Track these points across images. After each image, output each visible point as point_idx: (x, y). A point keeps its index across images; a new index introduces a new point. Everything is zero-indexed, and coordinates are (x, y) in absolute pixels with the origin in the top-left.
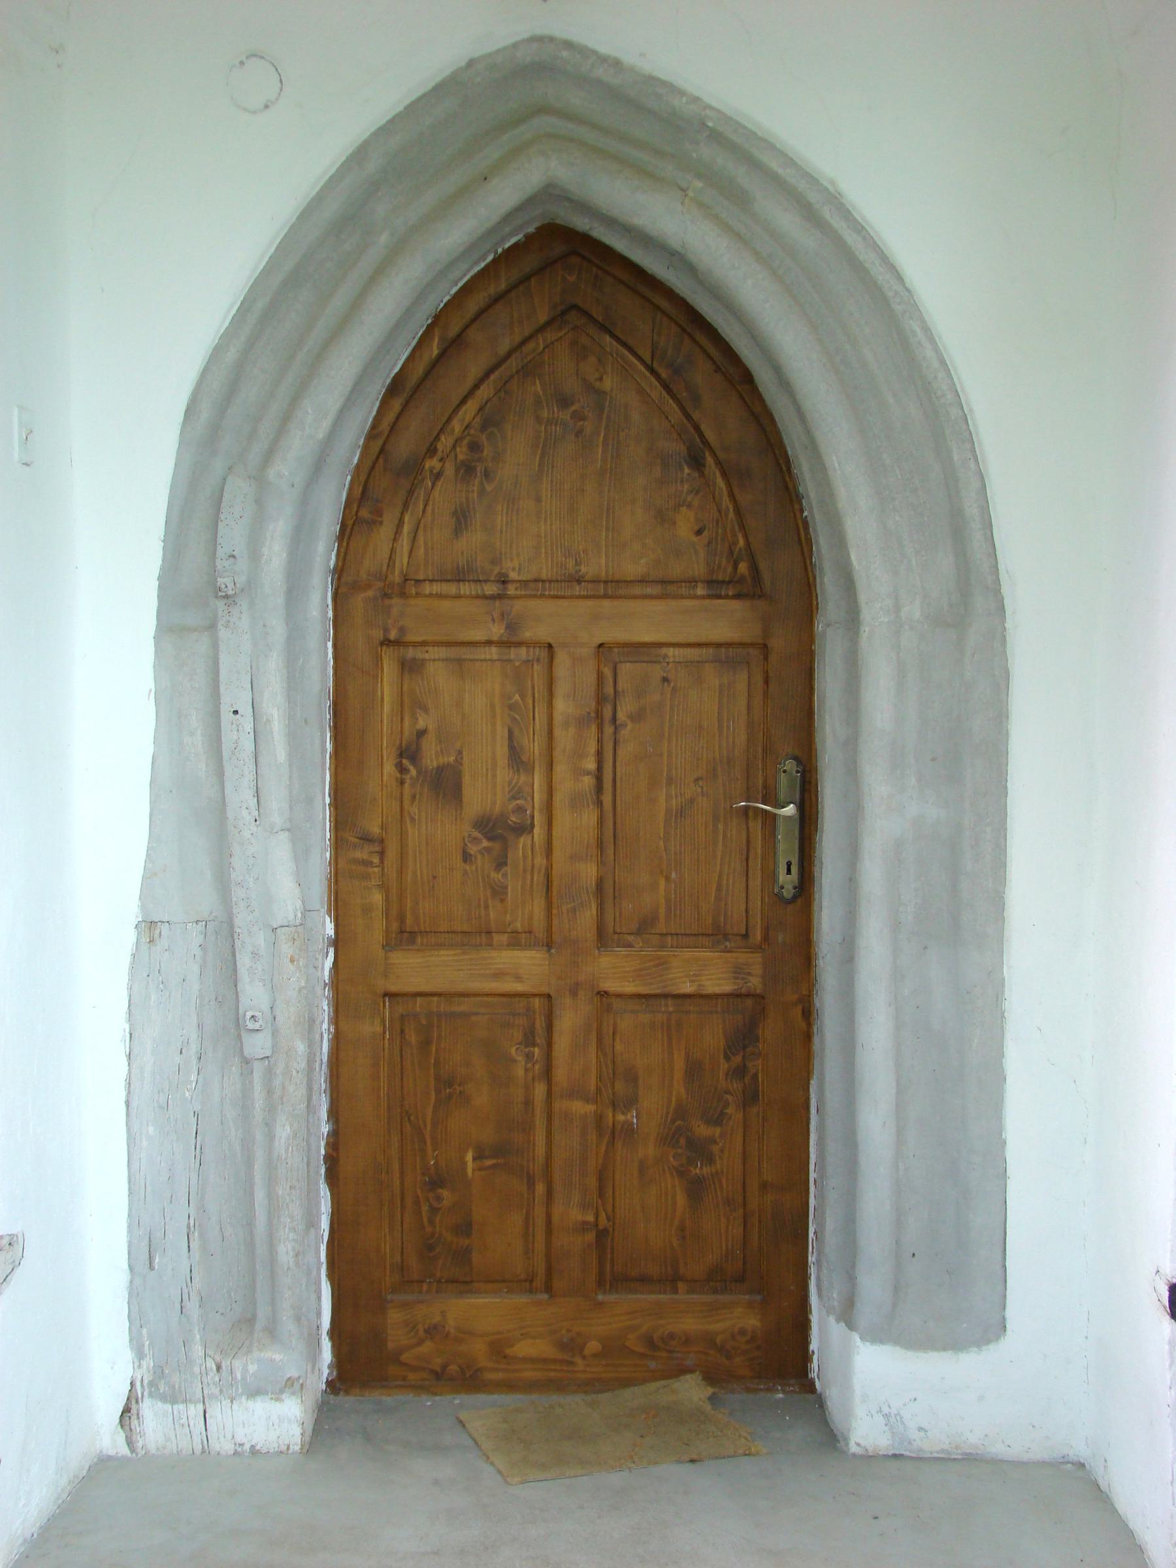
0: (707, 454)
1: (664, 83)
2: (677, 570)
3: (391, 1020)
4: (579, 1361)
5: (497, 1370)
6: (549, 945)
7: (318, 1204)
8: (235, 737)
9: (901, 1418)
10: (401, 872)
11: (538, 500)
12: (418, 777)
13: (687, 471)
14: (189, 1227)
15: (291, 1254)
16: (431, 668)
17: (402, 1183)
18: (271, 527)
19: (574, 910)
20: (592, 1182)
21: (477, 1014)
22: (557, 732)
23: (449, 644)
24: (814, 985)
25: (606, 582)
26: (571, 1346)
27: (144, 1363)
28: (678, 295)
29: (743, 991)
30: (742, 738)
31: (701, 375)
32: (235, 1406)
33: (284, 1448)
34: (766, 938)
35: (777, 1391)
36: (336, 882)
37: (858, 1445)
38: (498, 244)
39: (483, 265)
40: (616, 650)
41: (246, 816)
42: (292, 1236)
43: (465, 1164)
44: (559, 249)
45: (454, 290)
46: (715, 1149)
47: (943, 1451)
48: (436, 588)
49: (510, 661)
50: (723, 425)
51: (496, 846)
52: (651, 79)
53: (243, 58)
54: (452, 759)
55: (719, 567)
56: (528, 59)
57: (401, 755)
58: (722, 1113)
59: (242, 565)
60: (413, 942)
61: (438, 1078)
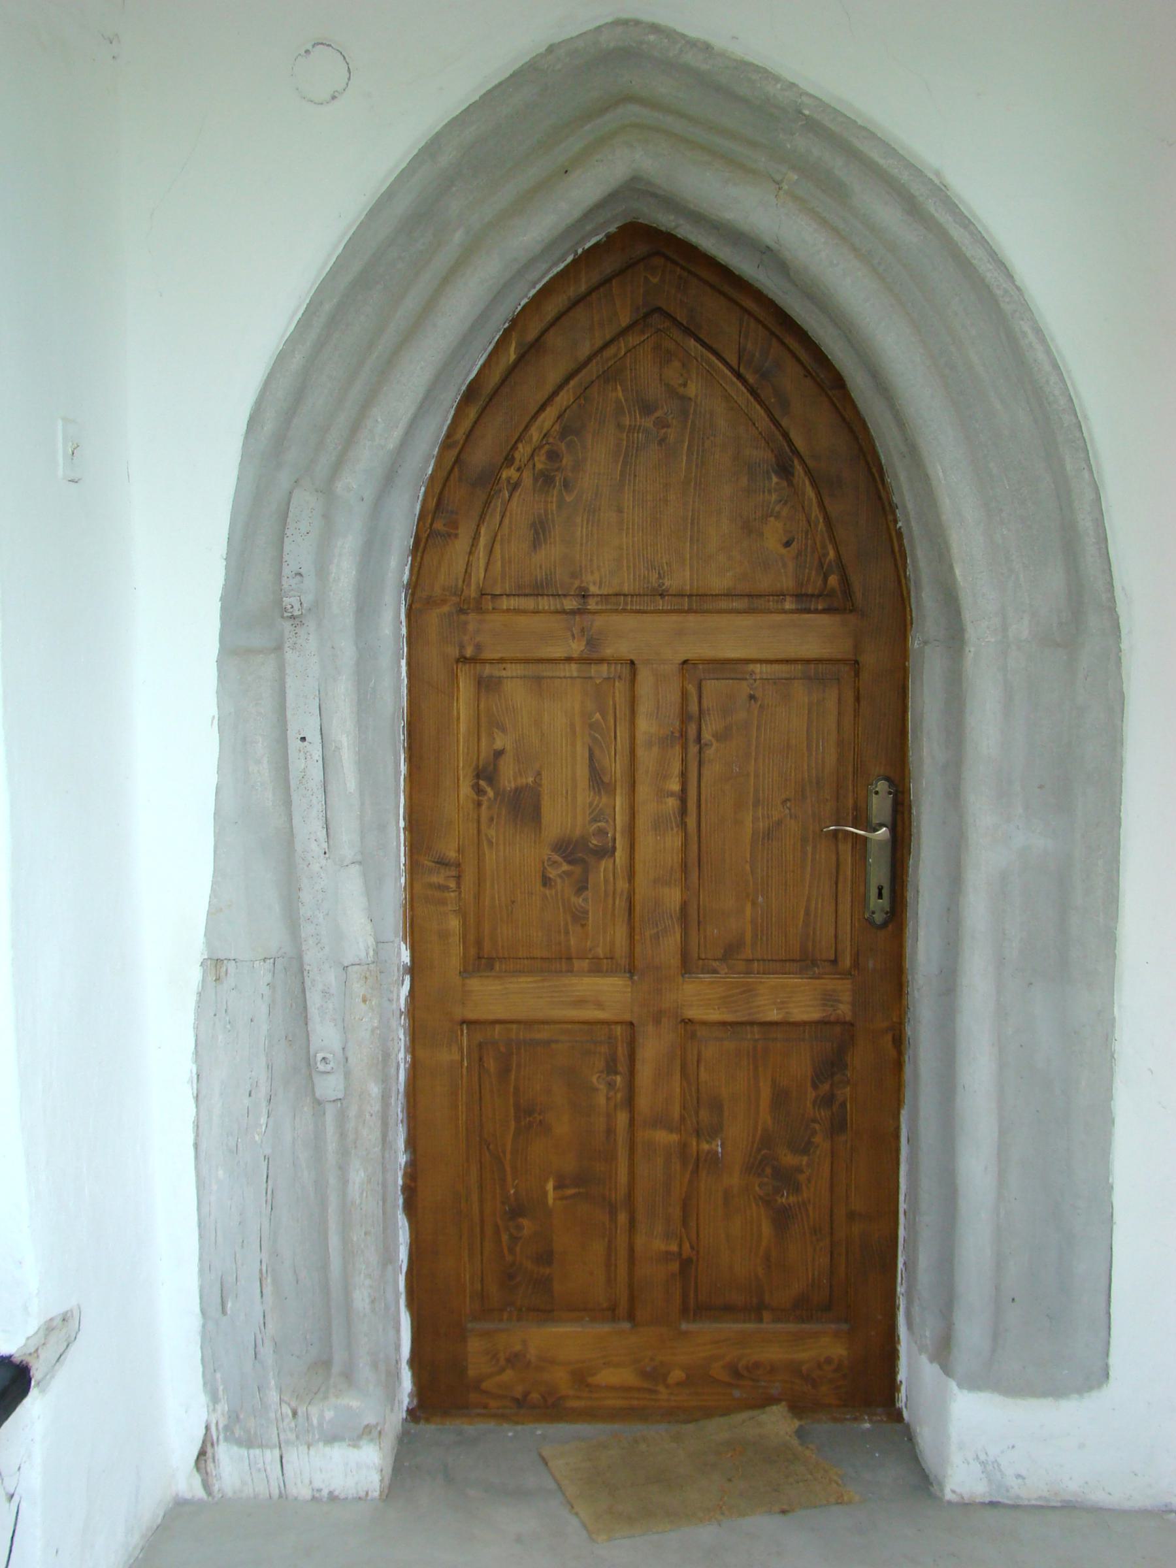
0: (796, 462)
1: (757, 69)
2: (764, 583)
3: (469, 1047)
4: (661, 1388)
5: (579, 1398)
6: (631, 971)
7: (396, 1236)
8: (303, 766)
9: (999, 1465)
10: (478, 897)
11: (620, 511)
12: (495, 799)
13: (775, 479)
14: (261, 1270)
15: (367, 1301)
16: (508, 686)
17: (482, 1212)
18: (339, 544)
19: (656, 937)
20: (677, 1213)
21: (557, 1042)
22: (640, 752)
23: (527, 661)
24: (905, 1013)
25: (690, 596)
26: (654, 1375)
27: (219, 1407)
28: (766, 297)
29: (832, 1018)
30: (831, 758)
31: (790, 380)
32: (312, 1452)
33: (362, 1494)
34: (856, 964)
35: (864, 1421)
36: (412, 908)
37: (953, 1492)
38: (578, 244)
39: (562, 266)
40: (701, 667)
41: (316, 849)
42: (368, 1282)
43: (545, 1193)
44: (641, 249)
45: (533, 292)
46: (802, 1178)
47: (1040, 1498)
48: (514, 603)
49: (591, 678)
50: (811, 430)
51: (577, 870)
52: (743, 66)
53: (309, 47)
54: (530, 780)
55: (808, 580)
56: (612, 45)
57: (478, 776)
58: (809, 1143)
59: (310, 582)
60: (492, 968)
61: (517, 1106)
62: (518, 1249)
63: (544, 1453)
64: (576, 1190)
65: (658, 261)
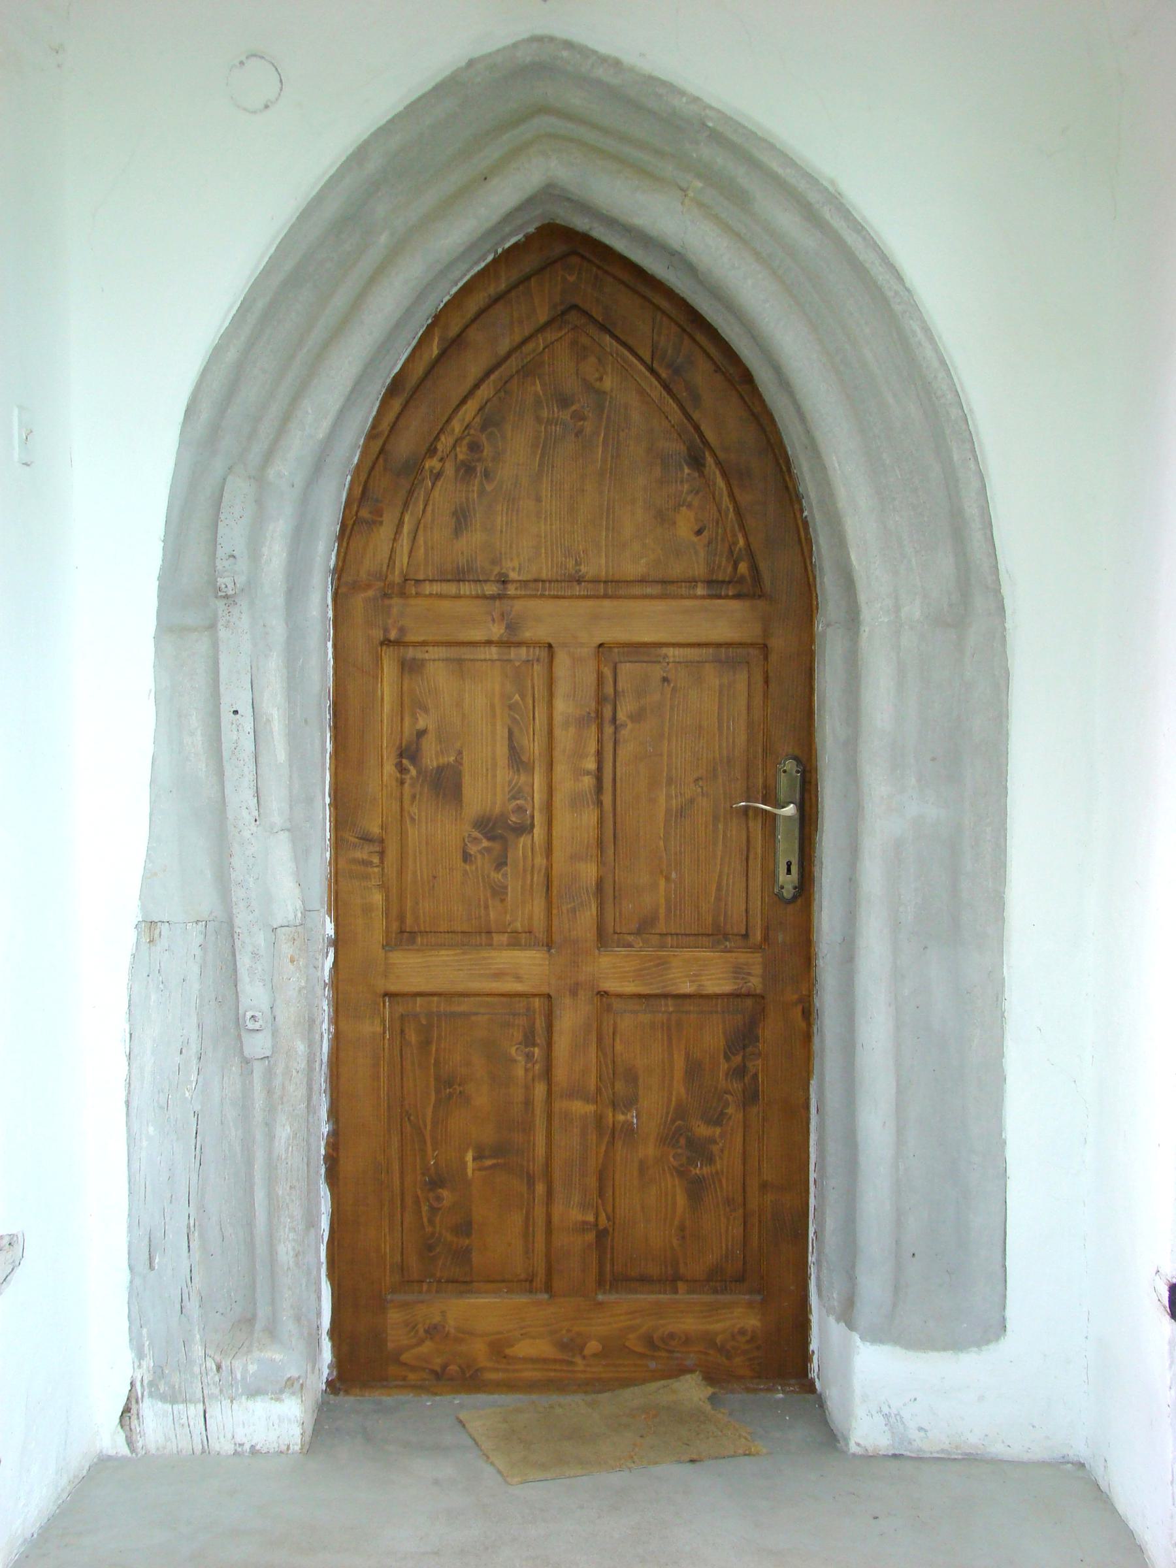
0: (707, 454)
1: (664, 83)
2: (676, 570)
3: (391, 1020)
4: (578, 1360)
5: (497, 1370)
6: (549, 945)
7: (318, 1204)
8: (235, 737)
9: (901, 1418)
11: (538, 499)
12: (418, 777)
13: (687, 470)
15: (291, 1253)
16: (431, 668)
17: (402, 1183)
18: (271, 528)
19: (574, 910)
20: (592, 1182)
21: (476, 1014)
22: (557, 732)
23: (449, 644)
24: (814, 985)
25: (606, 582)
26: (572, 1346)
27: (144, 1363)
28: (678, 295)
29: (744, 991)
30: (742, 738)
31: (701, 375)
32: (235, 1406)
33: (284, 1448)
34: (766, 938)
35: (777, 1391)
37: (858, 1445)
38: (498, 244)
39: (483, 265)
40: (616, 650)
41: (247, 817)
42: (291, 1235)
43: (465, 1164)
44: (559, 249)
45: (454, 290)
46: (715, 1149)
47: (943, 1451)
48: (436, 588)
50: (723, 424)
51: (497, 846)
52: (651, 80)
53: (243, 58)
54: (452, 759)
55: (719, 567)
56: (528, 59)
57: (401, 755)
58: (722, 1114)
59: (242, 565)
61: (438, 1078)
62: (438, 1219)
63: (461, 1417)
64: (495, 1161)
65: (574, 260)
